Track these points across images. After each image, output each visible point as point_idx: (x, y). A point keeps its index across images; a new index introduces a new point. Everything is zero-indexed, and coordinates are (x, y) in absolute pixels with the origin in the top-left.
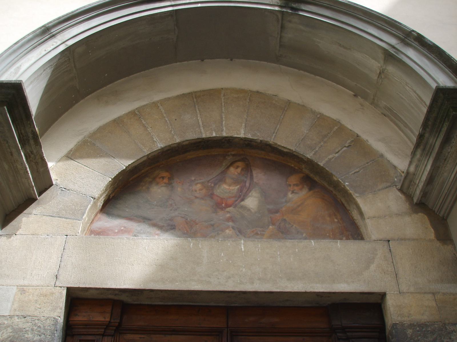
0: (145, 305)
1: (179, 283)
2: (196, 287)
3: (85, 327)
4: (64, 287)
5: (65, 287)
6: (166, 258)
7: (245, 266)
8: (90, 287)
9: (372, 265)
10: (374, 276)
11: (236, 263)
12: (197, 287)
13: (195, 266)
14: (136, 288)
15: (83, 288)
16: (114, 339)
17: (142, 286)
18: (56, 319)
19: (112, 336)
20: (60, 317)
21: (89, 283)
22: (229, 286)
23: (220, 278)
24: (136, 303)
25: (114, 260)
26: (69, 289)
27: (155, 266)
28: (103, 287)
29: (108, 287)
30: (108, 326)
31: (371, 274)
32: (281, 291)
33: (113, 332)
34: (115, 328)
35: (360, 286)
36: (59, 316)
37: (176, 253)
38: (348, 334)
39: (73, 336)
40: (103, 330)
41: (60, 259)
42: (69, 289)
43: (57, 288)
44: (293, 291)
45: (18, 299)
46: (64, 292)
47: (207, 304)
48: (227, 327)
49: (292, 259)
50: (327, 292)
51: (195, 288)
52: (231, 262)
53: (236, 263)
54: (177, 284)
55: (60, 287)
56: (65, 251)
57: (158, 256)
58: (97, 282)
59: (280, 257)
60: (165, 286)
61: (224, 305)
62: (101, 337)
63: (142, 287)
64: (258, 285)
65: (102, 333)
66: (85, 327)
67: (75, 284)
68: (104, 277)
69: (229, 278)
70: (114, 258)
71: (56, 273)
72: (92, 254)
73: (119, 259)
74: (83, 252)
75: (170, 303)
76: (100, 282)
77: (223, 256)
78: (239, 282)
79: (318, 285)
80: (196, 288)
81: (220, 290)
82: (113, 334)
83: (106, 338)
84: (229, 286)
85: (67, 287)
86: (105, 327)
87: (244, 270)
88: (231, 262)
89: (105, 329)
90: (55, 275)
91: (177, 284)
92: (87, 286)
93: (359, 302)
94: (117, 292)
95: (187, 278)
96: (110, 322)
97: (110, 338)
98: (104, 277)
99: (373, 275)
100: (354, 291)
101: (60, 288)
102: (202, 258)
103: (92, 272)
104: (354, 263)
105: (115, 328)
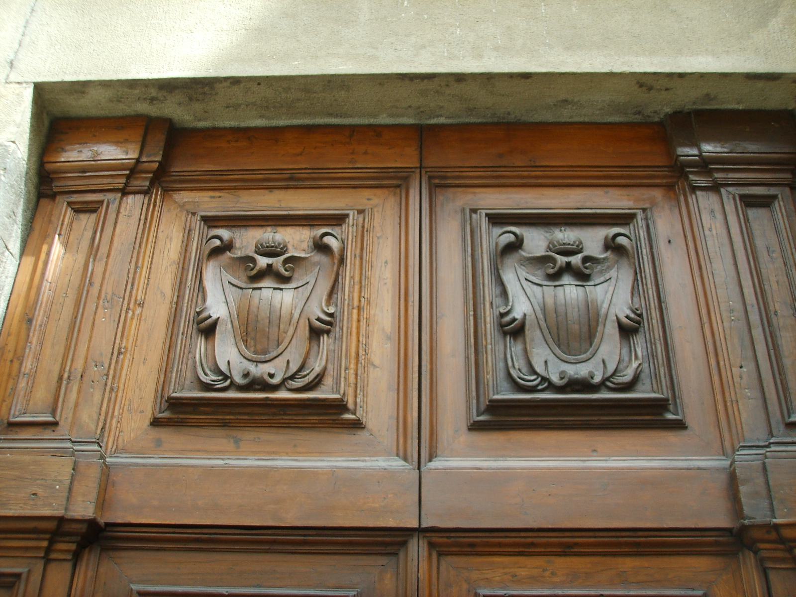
0: (225, 129)
1: (299, 62)
2: (340, 68)
3: (80, 175)
4: (27, 83)
5: (31, 82)
6: (271, 16)
7: (460, 23)
8: (88, 80)
9: (774, 20)
10: (778, 40)
11: (438, 18)
12: (345, 67)
13: (340, 27)
14: (196, 77)
15: (72, 82)
16: (150, 200)
17: (211, 71)
18: (5, 146)
19: (146, 193)
20: (13, 142)
21: (86, 72)
22: (421, 64)
23: (399, 48)
24: (201, 124)
25: (148, 25)
26: (39, 89)
27: (243, 31)
28: (120, 78)
29: (130, 78)
30: (134, 170)
31: (771, 36)
32: (552, 70)
33: (147, 183)
34: (151, 175)
35: (745, 61)
36: (13, 140)
37: (295, 5)
38: (716, 175)
39: (53, 196)
40: (124, 180)
41: (21, 30)
42: (39, 89)
43: (11, 85)
44: (579, 71)
45: (79, 499)
46: (28, 94)
47: (372, 121)
48: (421, 168)
49: (574, 9)
50: (664, 73)
51: (340, 69)
52: (426, 17)
53: (438, 18)
54: (296, 63)
55: (18, 83)
56: (34, 14)
57: (251, 12)
58: (105, 69)
59: (545, 5)
60: (268, 68)
61: (411, 121)
62: (120, 195)
63: (212, 73)
64: (493, 59)
65: (121, 186)
66: (80, 175)
67: (53, 75)
68: (123, 58)
69: (423, 47)
70: (149, 22)
71: (12, 57)
72: (97, 17)
73: (159, 24)
74: (75, 15)
75: (282, 122)
76: (113, 67)
77: (407, 7)
78: (446, 54)
79: (641, 59)
80: (343, 69)
81: (399, 72)
82: (146, 188)
83: (130, 199)
84: (421, 64)
85: (34, 83)
86: (128, 172)
87: (458, 32)
88: (426, 17)
89: (128, 177)
90: (9, 61)
91: (296, 64)
92: (82, 78)
93: (741, 107)
94: (154, 92)
95: (319, 50)
96: (138, 161)
97: (139, 197)
98: (123, 58)
99: (776, 38)
100: (732, 71)
101: (17, 86)
102: (357, 11)
103: (94, 50)
104: (728, 16)
105: (151, 175)
